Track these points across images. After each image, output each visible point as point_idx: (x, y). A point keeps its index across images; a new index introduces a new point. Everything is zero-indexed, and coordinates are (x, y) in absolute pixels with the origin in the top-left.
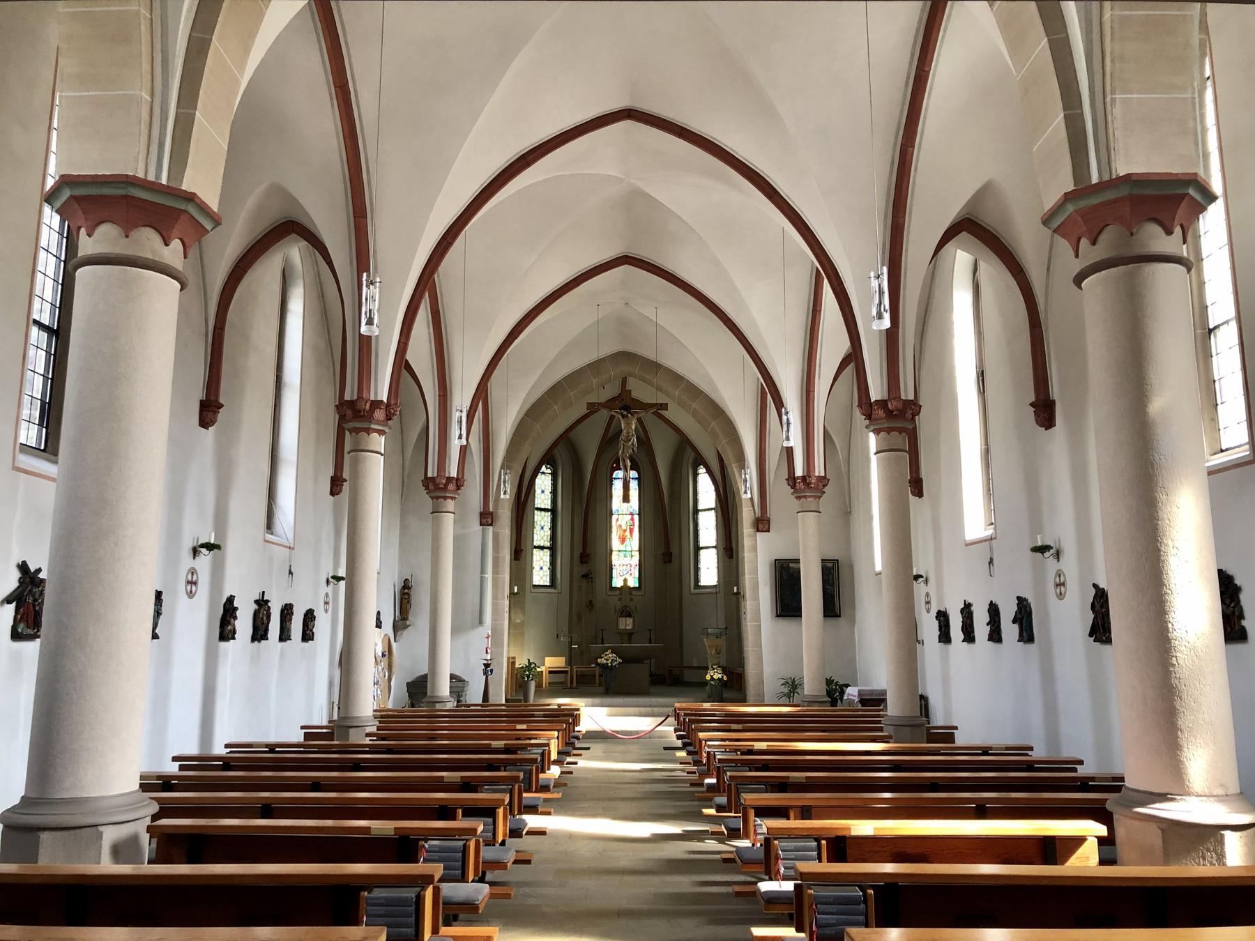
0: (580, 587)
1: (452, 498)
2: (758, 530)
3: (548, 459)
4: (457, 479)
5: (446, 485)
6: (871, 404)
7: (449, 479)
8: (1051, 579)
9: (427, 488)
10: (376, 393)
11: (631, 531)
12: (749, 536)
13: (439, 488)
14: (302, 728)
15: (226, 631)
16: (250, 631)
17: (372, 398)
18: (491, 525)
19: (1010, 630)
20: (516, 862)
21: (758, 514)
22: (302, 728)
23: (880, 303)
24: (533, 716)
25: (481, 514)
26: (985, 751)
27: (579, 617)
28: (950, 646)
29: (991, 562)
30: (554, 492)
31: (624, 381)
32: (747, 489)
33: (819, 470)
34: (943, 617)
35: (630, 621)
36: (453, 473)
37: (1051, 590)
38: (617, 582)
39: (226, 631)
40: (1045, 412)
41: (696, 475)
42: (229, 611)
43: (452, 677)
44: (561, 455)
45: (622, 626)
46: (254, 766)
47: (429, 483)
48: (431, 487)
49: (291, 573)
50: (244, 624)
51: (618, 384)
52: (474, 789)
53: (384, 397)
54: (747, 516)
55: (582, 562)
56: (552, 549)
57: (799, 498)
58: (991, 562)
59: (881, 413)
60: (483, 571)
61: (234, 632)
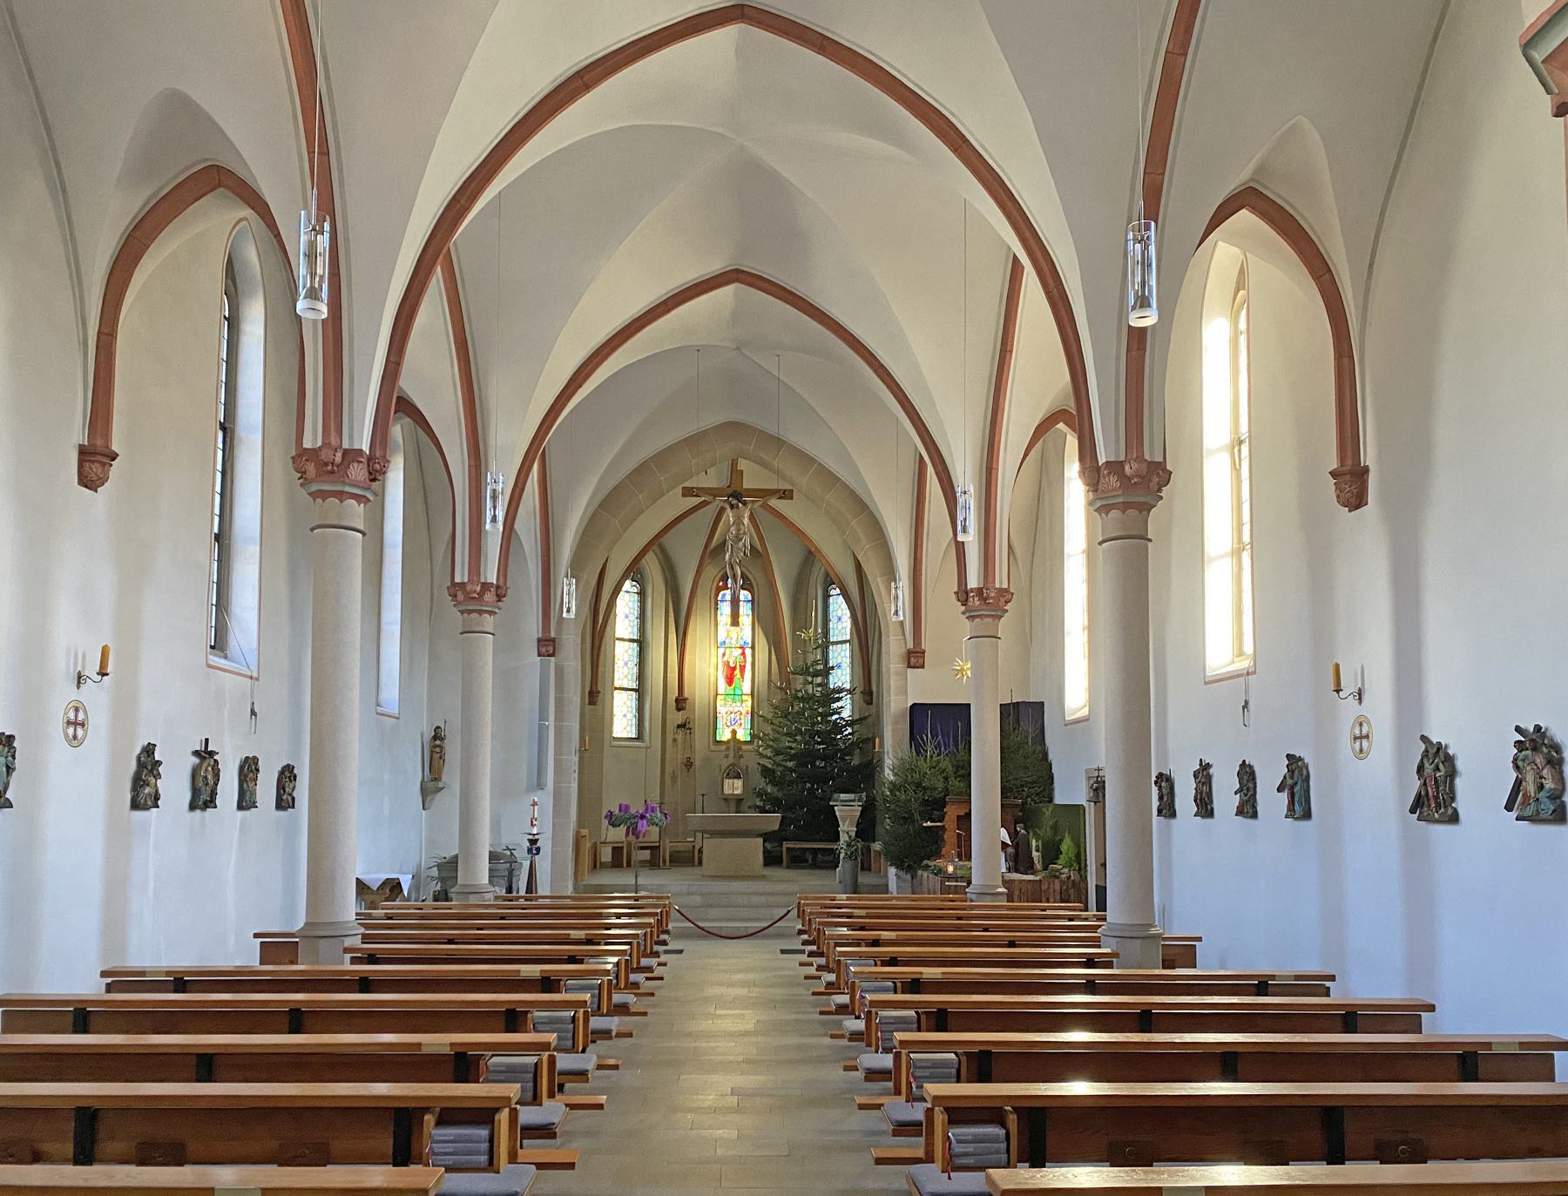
0: (675, 740)
1: (491, 613)
2: (909, 666)
3: (634, 571)
4: (498, 587)
5: (481, 594)
6: (1098, 469)
7: (486, 586)
8: (1346, 729)
9: (454, 596)
10: (351, 437)
11: (743, 669)
12: (898, 674)
13: (474, 598)
14: (256, 936)
15: (143, 792)
16: (187, 796)
17: (346, 445)
18: (553, 655)
19: (1271, 801)
20: (600, 1067)
21: (910, 645)
22: (256, 936)
23: (1143, 283)
24: (600, 916)
25: (539, 640)
26: (1262, 986)
27: (674, 778)
28: (1173, 821)
29: (1245, 706)
30: (642, 617)
31: (734, 464)
32: (895, 606)
33: (1001, 581)
34: (284, 801)
35: (738, 783)
36: (492, 577)
37: (1346, 746)
38: (724, 735)
39: (143, 792)
40: (1352, 485)
41: (827, 596)
42: (148, 765)
43: (493, 857)
44: (651, 565)
45: (727, 791)
46: (187, 997)
47: (455, 589)
48: (460, 597)
49: (253, 713)
50: (174, 784)
51: (725, 468)
52: (581, 962)
53: (366, 448)
54: (893, 648)
55: (679, 709)
56: (640, 691)
57: (972, 618)
58: (1245, 706)
59: (1113, 481)
60: (543, 716)
61: (157, 797)
